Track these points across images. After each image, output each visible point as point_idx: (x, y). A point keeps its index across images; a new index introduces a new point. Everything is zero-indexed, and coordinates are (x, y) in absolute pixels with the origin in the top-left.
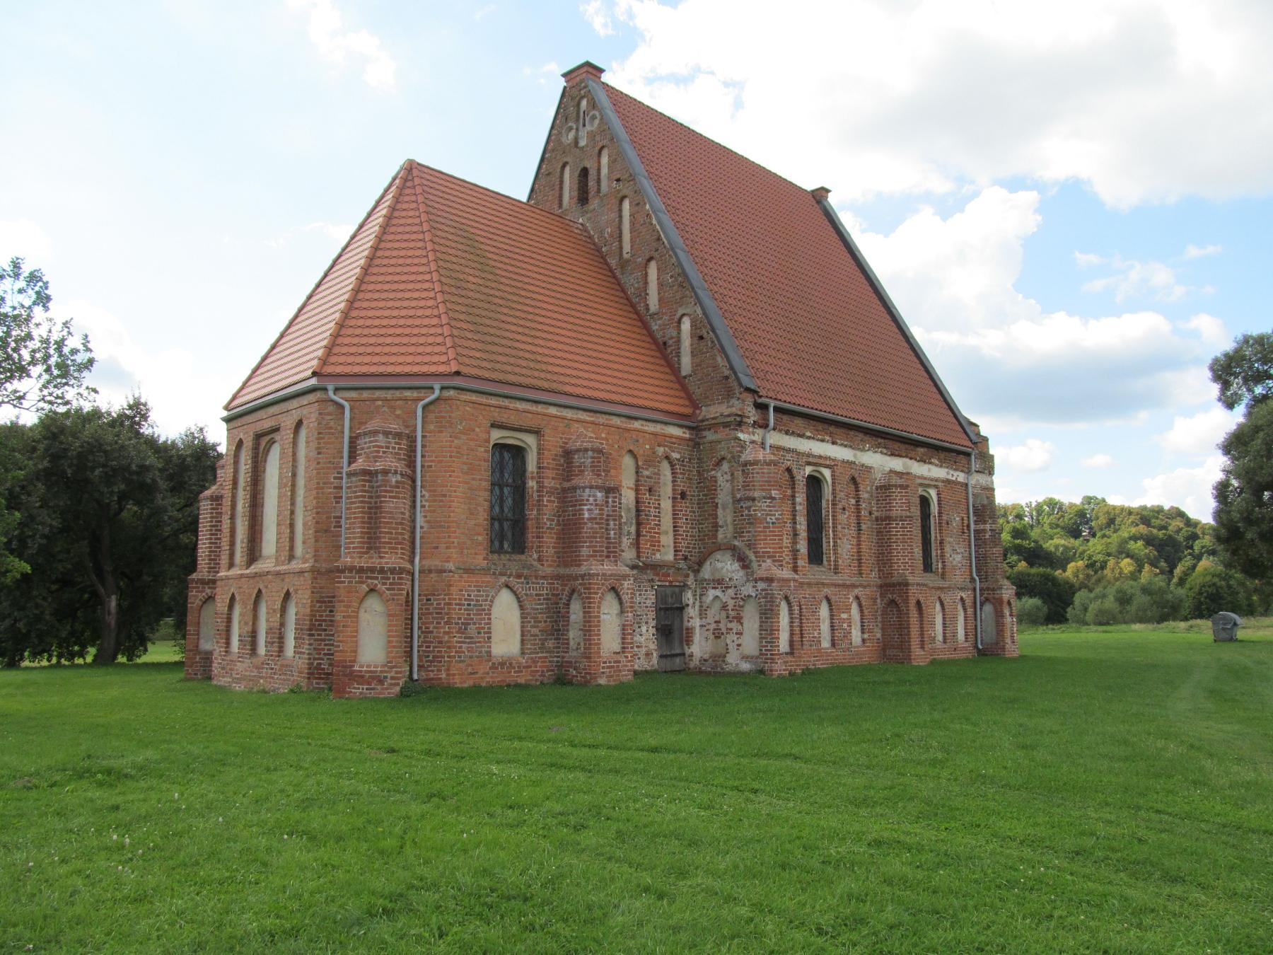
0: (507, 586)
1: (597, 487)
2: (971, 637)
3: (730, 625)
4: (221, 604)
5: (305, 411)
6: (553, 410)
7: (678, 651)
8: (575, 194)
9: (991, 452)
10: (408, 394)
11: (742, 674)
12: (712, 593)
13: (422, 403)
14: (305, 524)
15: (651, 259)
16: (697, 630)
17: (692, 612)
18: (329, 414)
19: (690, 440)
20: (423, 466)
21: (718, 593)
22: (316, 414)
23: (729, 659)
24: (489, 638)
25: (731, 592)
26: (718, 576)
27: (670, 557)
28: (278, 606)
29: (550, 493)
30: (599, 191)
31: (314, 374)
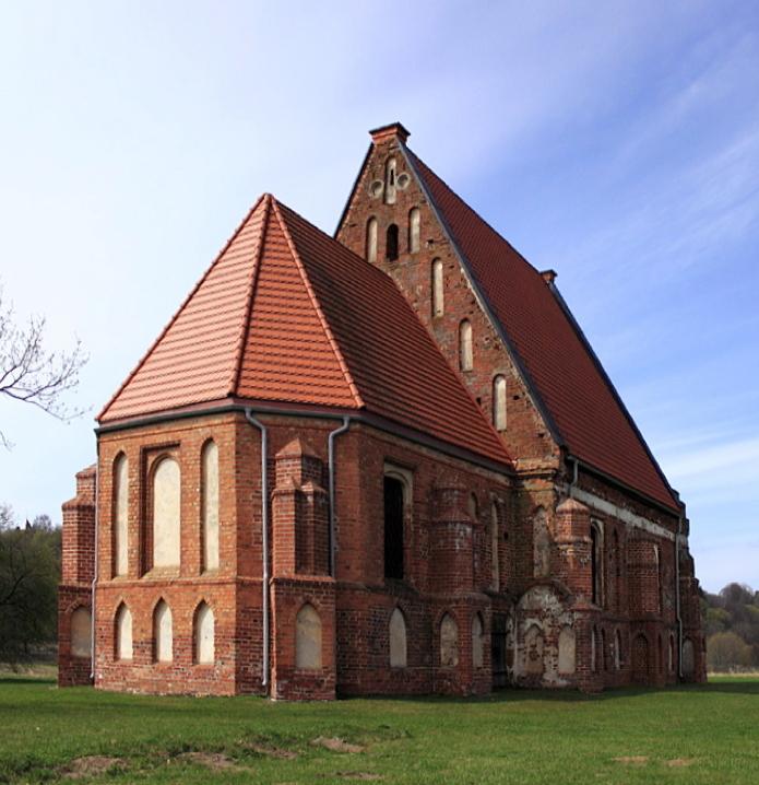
0: (399, 607)
1: (467, 523)
2: (676, 668)
3: (546, 649)
4: (103, 609)
5: (217, 430)
6: (424, 451)
7: (503, 670)
8: (384, 249)
9: (687, 517)
10: (318, 423)
11: (559, 689)
12: (529, 622)
13: (332, 434)
14: (221, 539)
15: (466, 320)
16: (516, 652)
17: (513, 637)
18: (246, 435)
19: (509, 488)
20: (334, 492)
21: (536, 621)
22: (234, 434)
23: (547, 677)
24: (389, 651)
25: (548, 621)
26: (535, 607)
27: (497, 589)
28: (190, 613)
29: (424, 526)
30: (409, 249)
31: (230, 395)
